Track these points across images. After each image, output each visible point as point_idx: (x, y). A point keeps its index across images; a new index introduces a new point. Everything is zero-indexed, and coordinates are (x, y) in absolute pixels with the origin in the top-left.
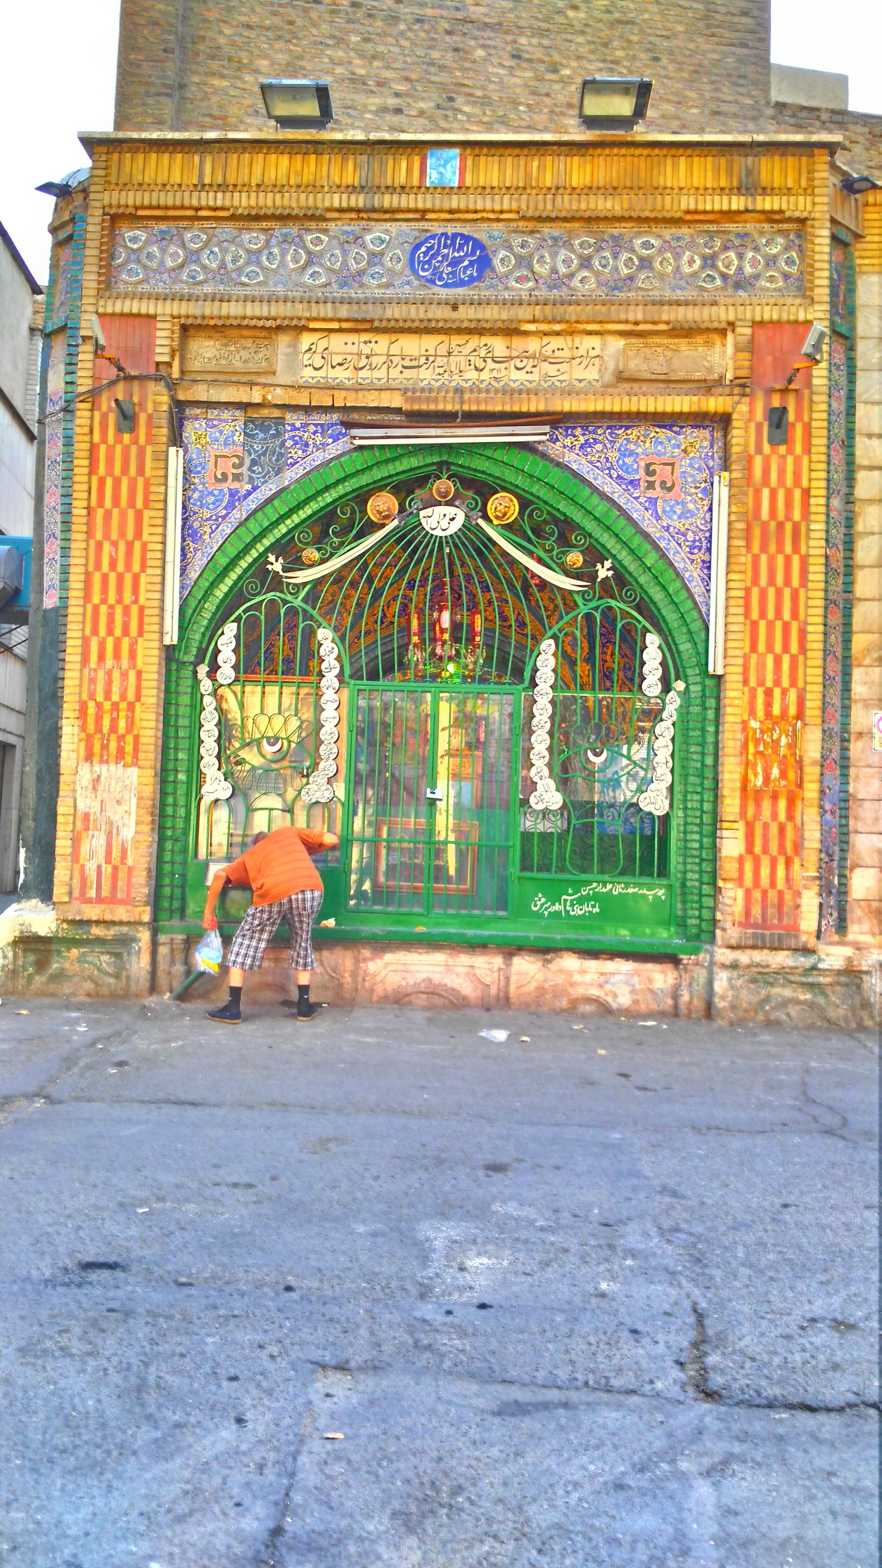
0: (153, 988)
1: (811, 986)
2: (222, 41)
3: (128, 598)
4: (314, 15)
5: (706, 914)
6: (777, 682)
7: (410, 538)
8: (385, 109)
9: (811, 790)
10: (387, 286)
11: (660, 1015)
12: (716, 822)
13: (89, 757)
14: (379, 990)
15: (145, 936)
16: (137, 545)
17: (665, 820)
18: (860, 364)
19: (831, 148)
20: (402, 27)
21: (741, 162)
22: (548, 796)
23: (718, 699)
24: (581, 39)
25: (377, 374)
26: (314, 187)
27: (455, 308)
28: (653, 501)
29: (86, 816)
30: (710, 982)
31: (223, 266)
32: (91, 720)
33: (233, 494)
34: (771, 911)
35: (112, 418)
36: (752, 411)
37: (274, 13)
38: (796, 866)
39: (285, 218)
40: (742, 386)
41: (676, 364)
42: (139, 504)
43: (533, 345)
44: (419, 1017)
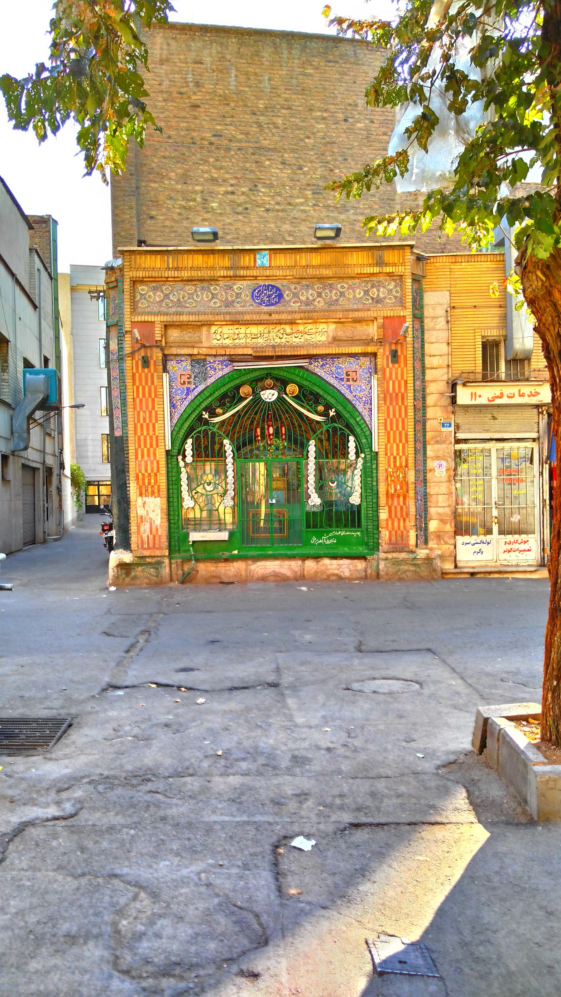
0: (171, 580)
1: (415, 565)
2: (154, 165)
3: (151, 433)
4: (193, 150)
5: (376, 541)
6: (398, 454)
7: (257, 400)
8: (227, 193)
9: (411, 493)
10: (244, 306)
11: (361, 579)
12: (377, 507)
13: (141, 495)
14: (256, 576)
15: (167, 561)
16: (153, 412)
17: (359, 506)
18: (426, 328)
19: (412, 247)
20: (232, 153)
21: (377, 253)
22: (315, 500)
23: (377, 460)
24: (312, 153)
25: (242, 341)
26: (213, 268)
27: (270, 315)
28: (349, 386)
29: (142, 517)
30: (378, 565)
31: (179, 300)
32: (140, 480)
33: (188, 389)
34: (399, 538)
35: (140, 363)
36: (384, 352)
37: (175, 150)
38: (407, 522)
39: (202, 280)
40: (380, 342)
41: (356, 333)
42: (153, 396)
43: (301, 328)
44: (272, 585)
